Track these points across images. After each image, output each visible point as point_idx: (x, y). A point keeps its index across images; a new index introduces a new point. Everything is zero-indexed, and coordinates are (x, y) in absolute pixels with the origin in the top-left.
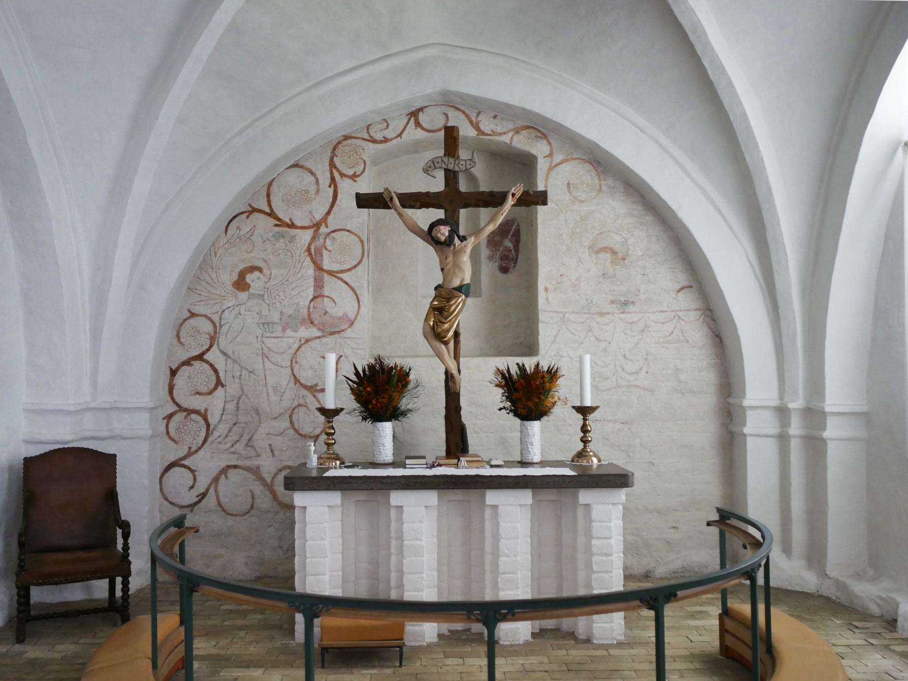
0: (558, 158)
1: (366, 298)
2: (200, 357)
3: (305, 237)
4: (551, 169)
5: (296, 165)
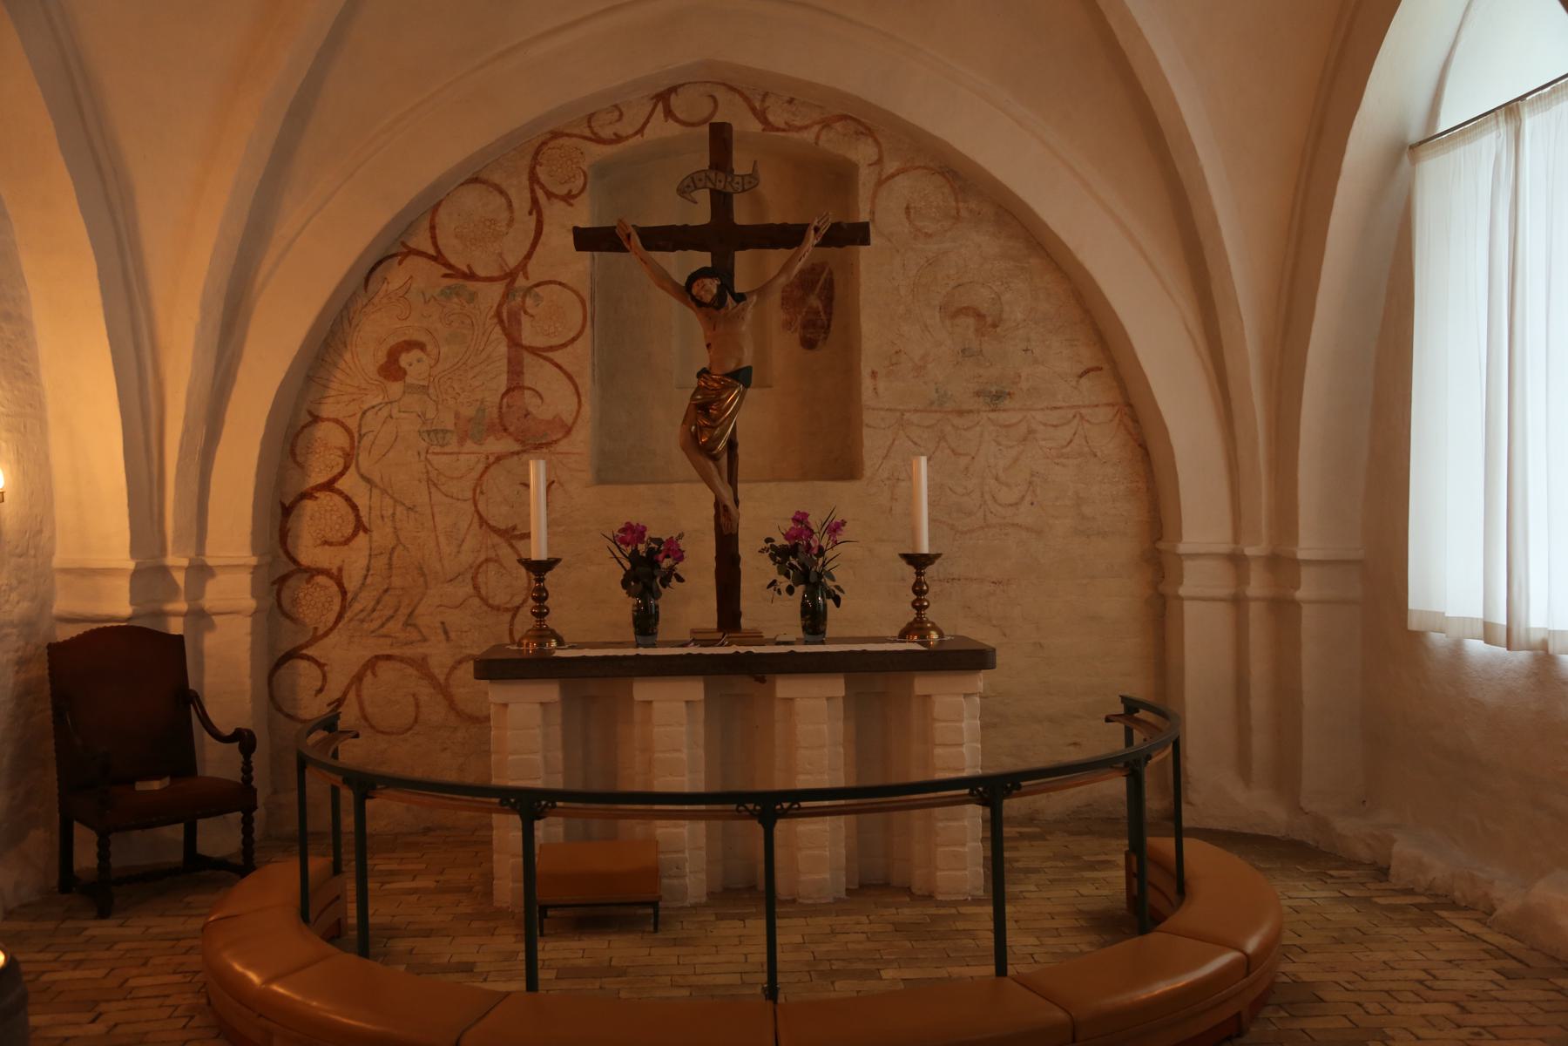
0: (891, 166)
1: (586, 383)
2: (329, 486)
3: (491, 294)
4: (880, 183)
5: (475, 180)
